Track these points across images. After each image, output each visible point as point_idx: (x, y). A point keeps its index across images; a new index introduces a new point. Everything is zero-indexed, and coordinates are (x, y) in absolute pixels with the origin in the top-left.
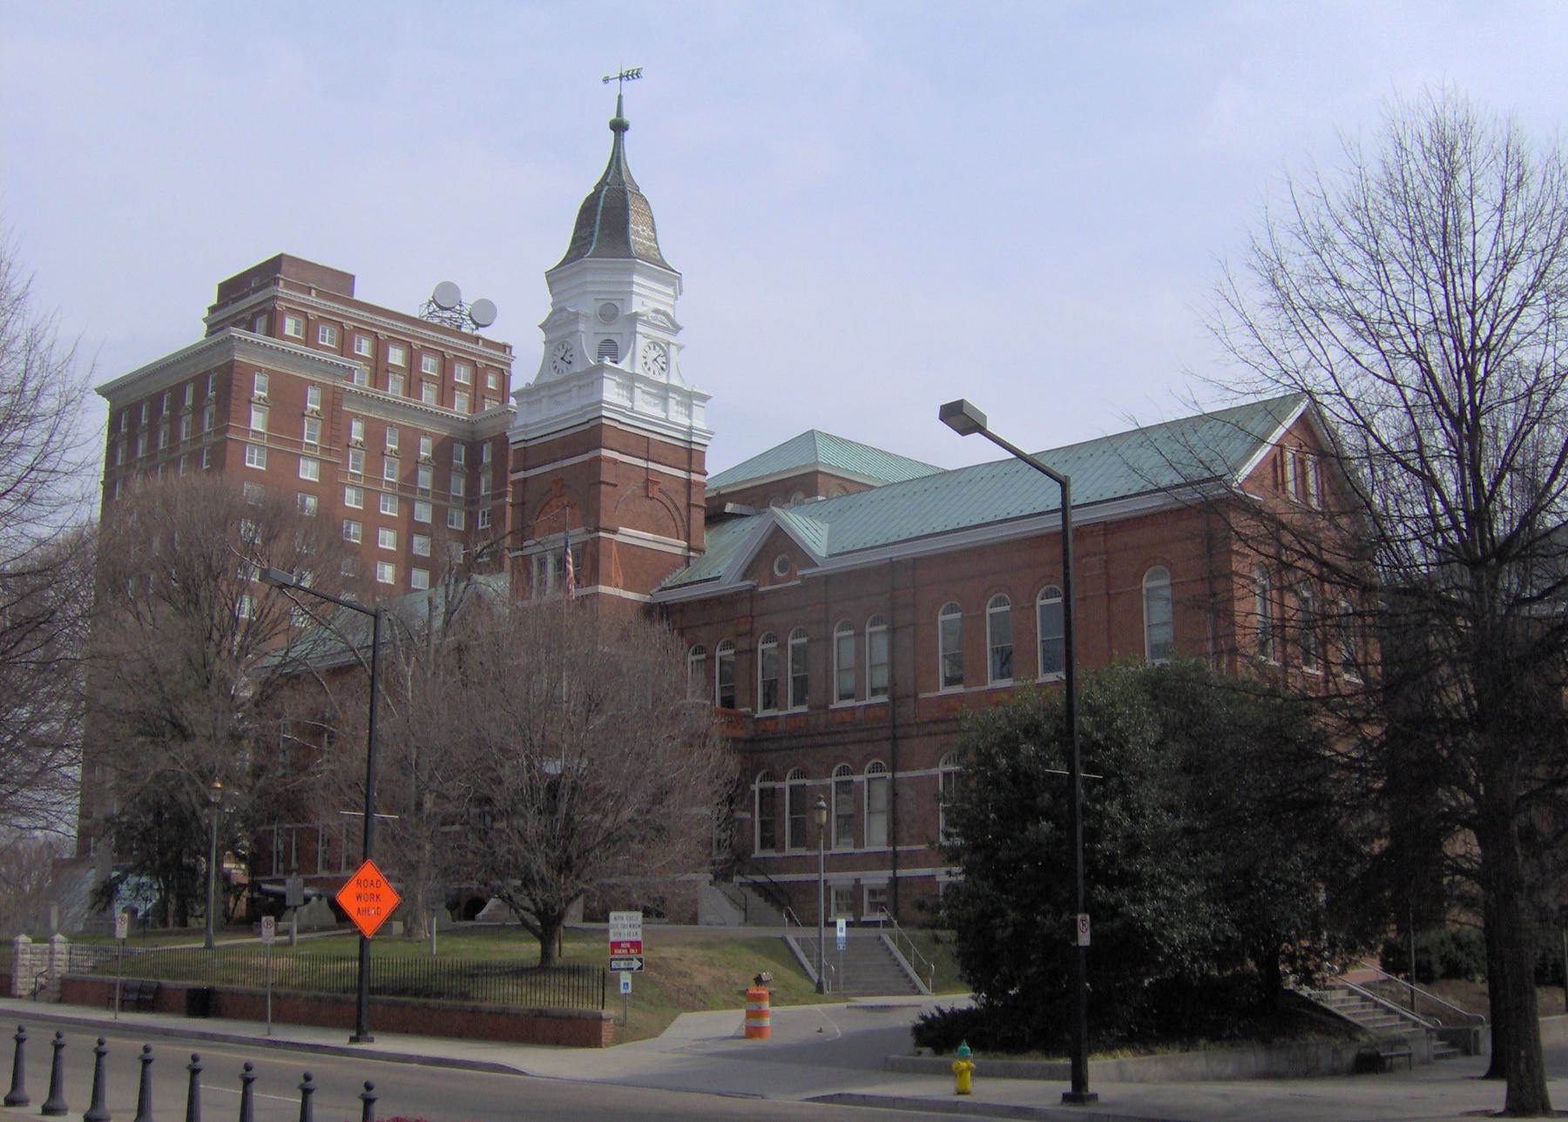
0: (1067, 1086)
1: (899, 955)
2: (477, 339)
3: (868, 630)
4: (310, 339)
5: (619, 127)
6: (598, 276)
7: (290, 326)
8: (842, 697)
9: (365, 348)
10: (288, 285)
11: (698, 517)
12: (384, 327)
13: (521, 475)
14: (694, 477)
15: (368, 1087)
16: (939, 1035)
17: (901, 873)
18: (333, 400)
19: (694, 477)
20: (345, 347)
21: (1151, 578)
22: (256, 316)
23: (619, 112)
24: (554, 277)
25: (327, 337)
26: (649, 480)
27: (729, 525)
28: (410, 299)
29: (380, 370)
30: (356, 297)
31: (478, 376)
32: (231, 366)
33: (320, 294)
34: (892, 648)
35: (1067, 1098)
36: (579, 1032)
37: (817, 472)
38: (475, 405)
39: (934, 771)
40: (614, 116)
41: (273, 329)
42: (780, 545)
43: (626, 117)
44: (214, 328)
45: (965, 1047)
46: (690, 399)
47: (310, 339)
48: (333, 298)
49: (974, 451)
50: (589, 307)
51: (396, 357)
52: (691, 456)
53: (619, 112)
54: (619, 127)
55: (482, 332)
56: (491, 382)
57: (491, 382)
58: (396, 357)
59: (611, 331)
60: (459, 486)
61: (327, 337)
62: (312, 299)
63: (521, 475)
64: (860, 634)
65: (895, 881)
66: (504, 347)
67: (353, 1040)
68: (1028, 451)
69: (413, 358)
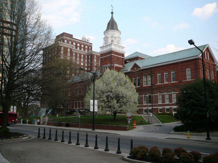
0: (207, 137)
1: (156, 118)
2: (88, 43)
3: (148, 76)
4: (68, 43)
5: (112, 13)
6: (111, 32)
7: (65, 41)
8: (188, 79)
9: (74, 44)
10: (65, 36)
11: (124, 63)
12: (77, 42)
13: (101, 57)
14: (123, 57)
15: (132, 140)
16: (177, 129)
17: (153, 107)
18: (71, 50)
19: (123, 57)
20: (72, 44)
21: (188, 69)
22: (61, 40)
23: (112, 11)
24: (105, 33)
25: (70, 42)
26: (118, 58)
27: (127, 64)
28: (80, 38)
29: (76, 47)
30: (73, 37)
31: (88, 47)
32: (59, 46)
33: (69, 37)
34: (151, 79)
35: (206, 139)
36: (125, 129)
37: (138, 57)
38: (88, 51)
39: (157, 94)
40: (111, 12)
41: (64, 41)
42: (136, 66)
43: (113, 12)
44: (56, 42)
45: (188, 131)
46: (123, 47)
47: (68, 43)
48: (71, 38)
49: (192, 46)
50: (110, 36)
51: (78, 45)
52: (123, 55)
53: (112, 11)
54: (112, 13)
55: (88, 42)
56: (90, 48)
57: (90, 48)
58: (78, 45)
59: (112, 39)
60: (86, 61)
61: (70, 42)
62: (68, 38)
63: (101, 57)
64: (147, 77)
65: (152, 108)
66: (91, 44)
67: (92, 130)
68: (197, 46)
69: (80, 45)
